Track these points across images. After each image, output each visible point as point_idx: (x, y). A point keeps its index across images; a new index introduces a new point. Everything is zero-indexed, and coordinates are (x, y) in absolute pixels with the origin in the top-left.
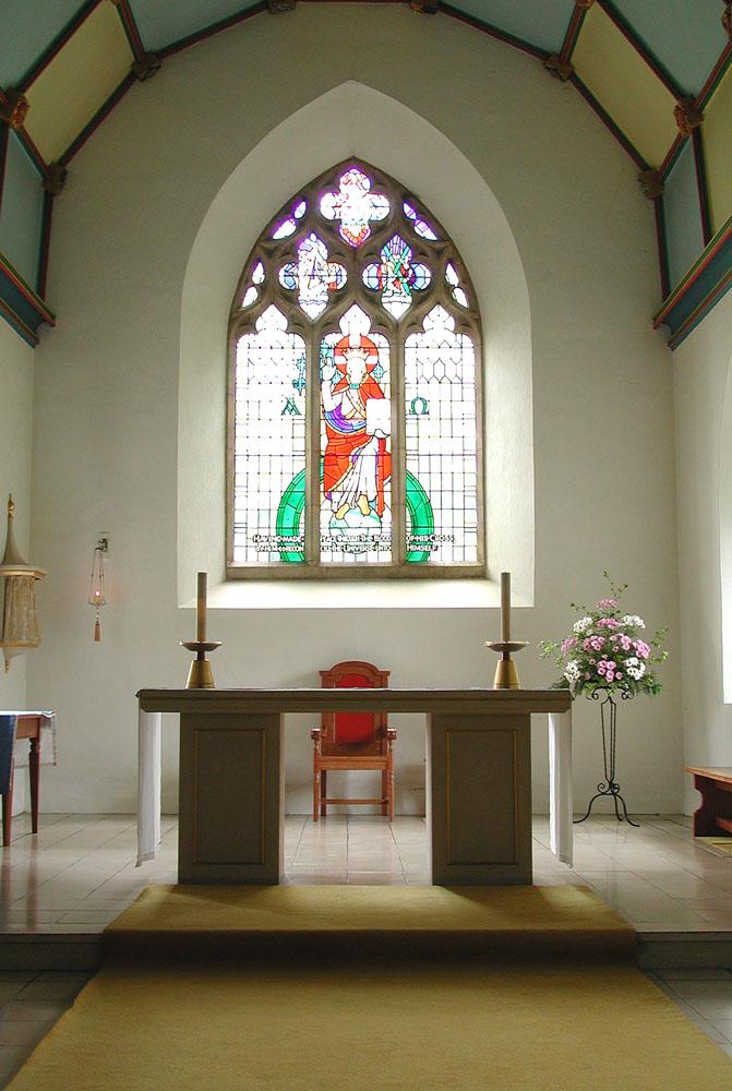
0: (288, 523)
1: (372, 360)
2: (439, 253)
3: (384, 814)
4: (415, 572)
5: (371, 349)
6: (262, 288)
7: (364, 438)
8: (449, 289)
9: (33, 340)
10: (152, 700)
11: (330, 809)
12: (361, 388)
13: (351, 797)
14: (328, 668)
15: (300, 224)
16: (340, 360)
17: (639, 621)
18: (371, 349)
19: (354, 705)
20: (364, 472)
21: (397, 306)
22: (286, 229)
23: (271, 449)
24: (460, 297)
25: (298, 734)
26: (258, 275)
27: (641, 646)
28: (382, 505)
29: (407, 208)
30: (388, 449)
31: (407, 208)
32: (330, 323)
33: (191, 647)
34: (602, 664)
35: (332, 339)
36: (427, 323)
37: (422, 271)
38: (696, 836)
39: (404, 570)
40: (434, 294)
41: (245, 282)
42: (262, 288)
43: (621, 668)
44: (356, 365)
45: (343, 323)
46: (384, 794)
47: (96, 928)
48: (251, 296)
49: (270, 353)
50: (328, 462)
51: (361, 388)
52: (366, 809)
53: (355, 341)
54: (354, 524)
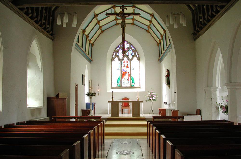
0: (118, 82)
1: (128, 63)
2: (135, 51)
3: (129, 113)
4: (132, 87)
5: (127, 62)
6: (115, 55)
7: (127, 72)
8: (136, 55)
9: (91, 63)
10: (109, 102)
11: (123, 113)
12: (126, 67)
13: (125, 112)
14: (123, 98)
15: (119, 48)
16: (124, 63)
17: (155, 93)
18: (127, 62)
19: (126, 102)
20: (126, 76)
21: (130, 57)
22: (118, 49)
23: (117, 74)
24: (137, 56)
25: (121, 104)
26: (115, 54)
27: (155, 96)
28: (129, 80)
29: (131, 46)
30: (129, 74)
31: (131, 46)
32: (123, 59)
33: (112, 97)
34: (151, 98)
35: (123, 61)
36: (134, 59)
37: (133, 53)
38: (159, 114)
39: (131, 87)
40: (135, 56)
41: (113, 55)
42: (115, 55)
43: (153, 98)
44: (126, 64)
45: (124, 59)
46: (129, 111)
47: (107, 118)
48: (114, 56)
49: (116, 62)
50: (123, 74)
51: (126, 67)
52: (127, 113)
53: (126, 61)
54: (126, 82)
